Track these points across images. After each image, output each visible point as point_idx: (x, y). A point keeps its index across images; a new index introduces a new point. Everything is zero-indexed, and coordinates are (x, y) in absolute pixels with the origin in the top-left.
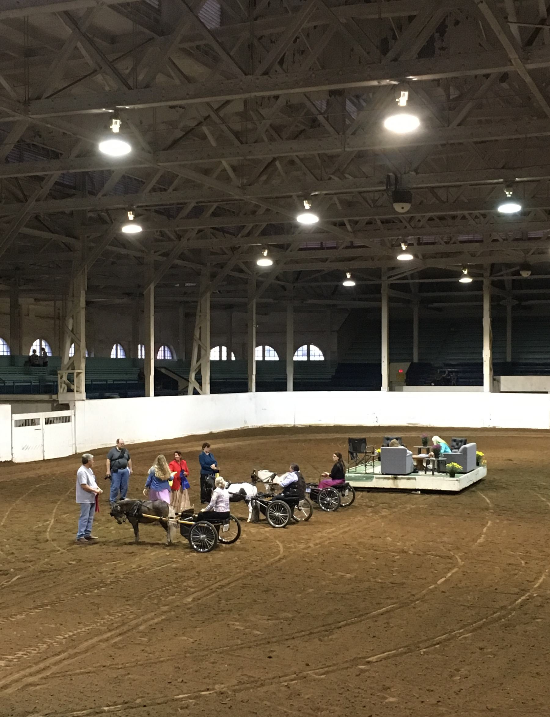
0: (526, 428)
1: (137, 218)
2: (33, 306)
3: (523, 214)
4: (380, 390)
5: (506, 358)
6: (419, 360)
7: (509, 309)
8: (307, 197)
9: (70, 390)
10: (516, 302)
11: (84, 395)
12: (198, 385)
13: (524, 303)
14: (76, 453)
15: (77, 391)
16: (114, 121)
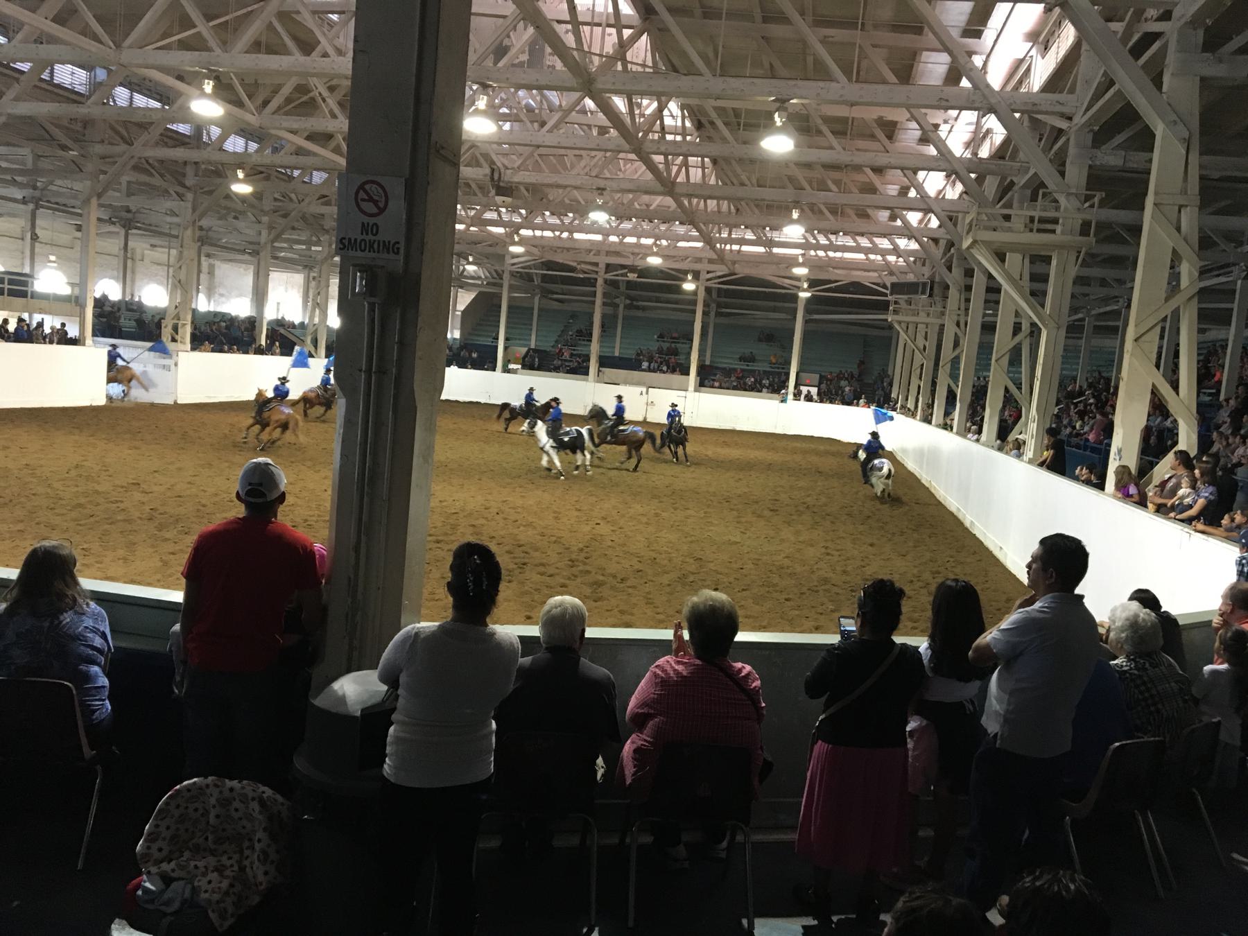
0: (779, 430)
1: (248, 178)
2: (149, 252)
3: (254, 194)
4: (495, 370)
5: (614, 352)
6: (536, 346)
7: (622, 306)
8: (797, 204)
9: (174, 340)
10: (628, 302)
11: (188, 346)
12: (313, 348)
13: (635, 303)
14: (175, 402)
15: (181, 342)
16: (206, 81)
